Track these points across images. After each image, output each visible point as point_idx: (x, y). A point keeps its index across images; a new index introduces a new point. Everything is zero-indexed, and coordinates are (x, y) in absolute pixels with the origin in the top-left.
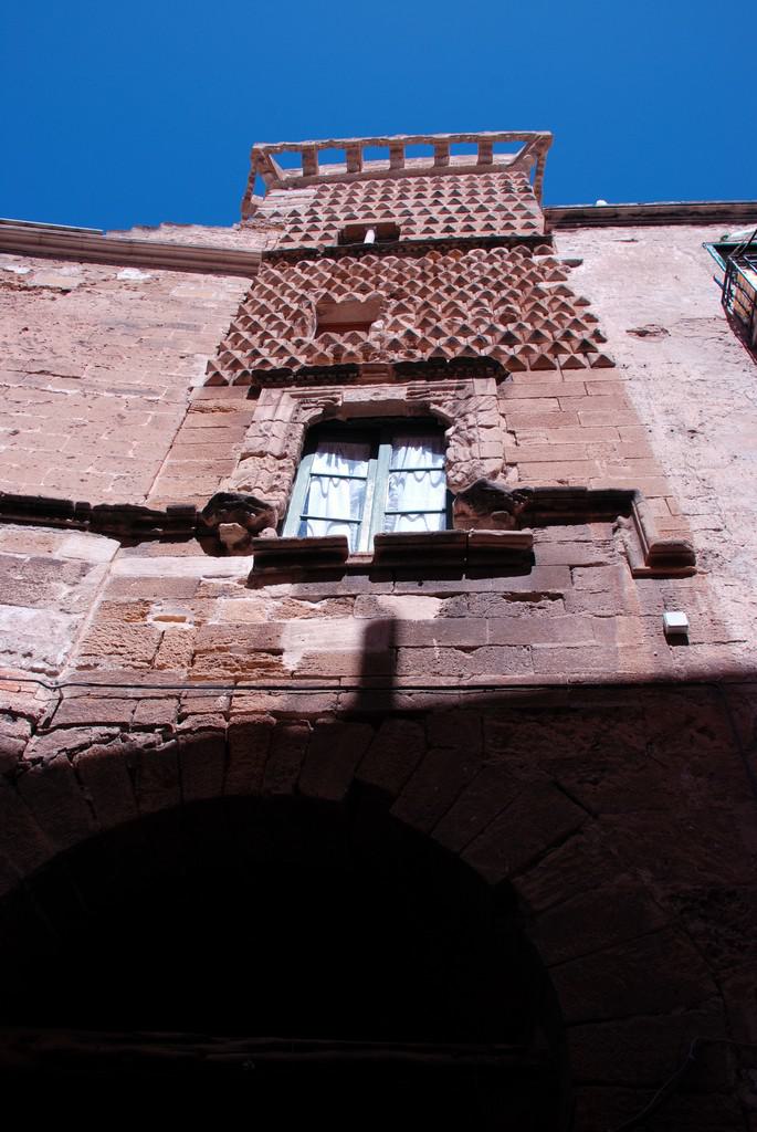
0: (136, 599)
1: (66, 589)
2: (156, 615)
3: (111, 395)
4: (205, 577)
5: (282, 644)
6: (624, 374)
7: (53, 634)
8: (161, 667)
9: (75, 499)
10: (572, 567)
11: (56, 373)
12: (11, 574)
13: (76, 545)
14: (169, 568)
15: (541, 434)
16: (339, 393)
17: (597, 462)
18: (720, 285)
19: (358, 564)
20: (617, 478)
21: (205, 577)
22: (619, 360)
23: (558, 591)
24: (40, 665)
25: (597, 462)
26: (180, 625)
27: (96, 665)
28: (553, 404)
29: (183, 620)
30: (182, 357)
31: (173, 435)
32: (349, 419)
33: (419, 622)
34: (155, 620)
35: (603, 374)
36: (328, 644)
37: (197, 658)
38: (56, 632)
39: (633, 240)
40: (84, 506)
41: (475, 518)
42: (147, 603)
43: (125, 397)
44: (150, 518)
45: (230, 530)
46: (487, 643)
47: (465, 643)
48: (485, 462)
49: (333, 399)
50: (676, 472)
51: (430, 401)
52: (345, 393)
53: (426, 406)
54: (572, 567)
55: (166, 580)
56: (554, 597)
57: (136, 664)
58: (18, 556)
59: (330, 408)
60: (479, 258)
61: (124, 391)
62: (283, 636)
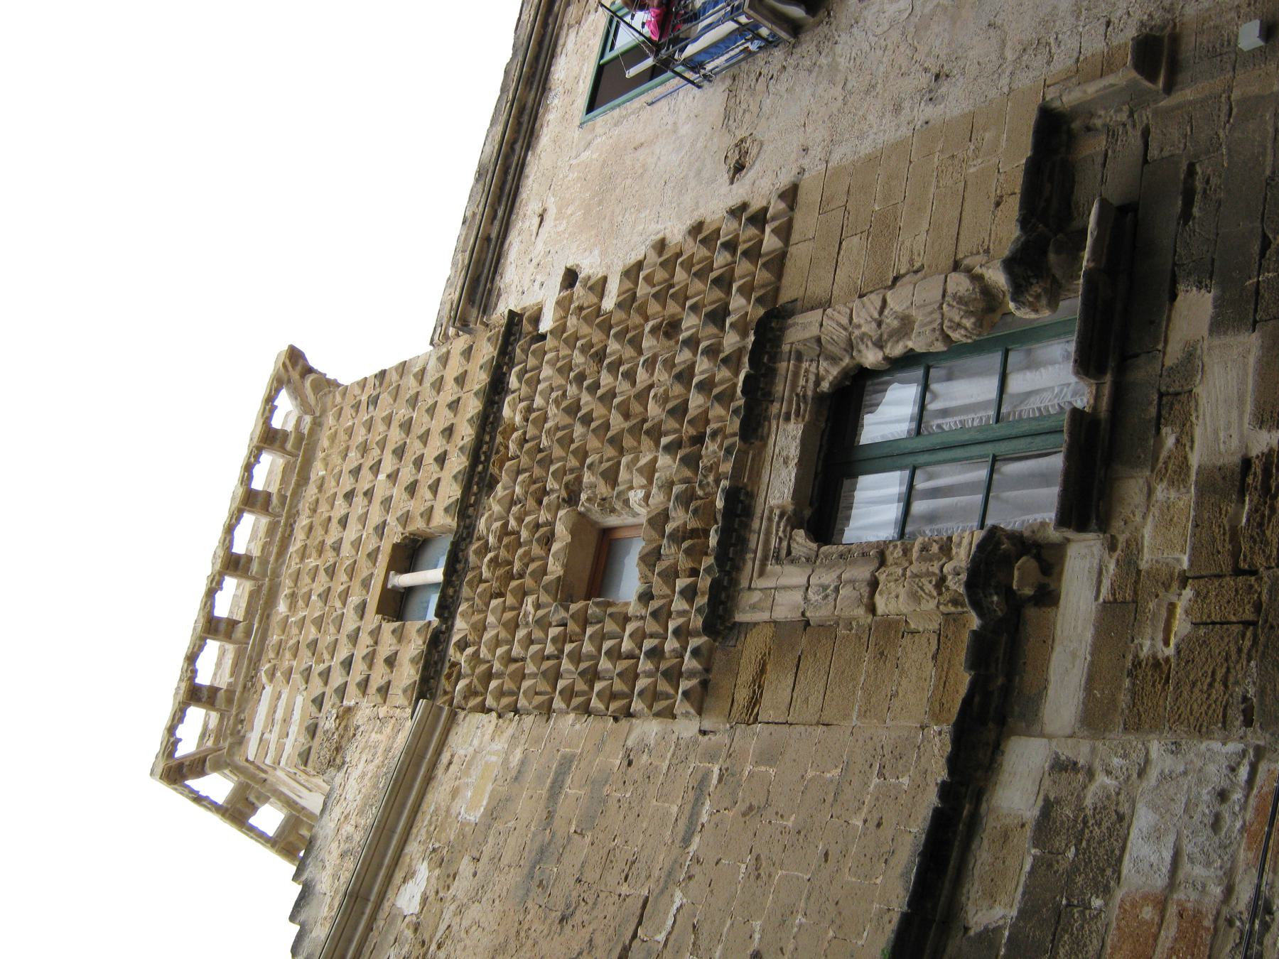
1: (1102, 779)
2: (1160, 644)
3: (696, 839)
4: (1097, 598)
5: (1237, 459)
6: (814, 167)
8: (1258, 607)
9: (931, 798)
11: (629, 934)
12: (1063, 866)
13: (1018, 788)
14: (1074, 655)
15: (907, 244)
16: (771, 511)
17: (972, 170)
20: (1004, 144)
21: (1097, 598)
23: (1185, 168)
24: (1244, 772)
25: (972, 170)
29: (1172, 607)
30: (630, 764)
32: (811, 504)
33: (1215, 307)
35: (809, 196)
36: (1241, 401)
37: (1244, 566)
39: (542, 217)
40: (946, 791)
42: (1137, 664)
44: (977, 699)
45: (1022, 576)
46: (1258, 224)
47: (1256, 248)
49: (781, 516)
50: (1005, 81)
52: (773, 502)
53: (820, 398)
54: (1145, 161)
56: (1191, 172)
57: (1248, 643)
58: (1027, 867)
61: (694, 815)
62: (1219, 464)
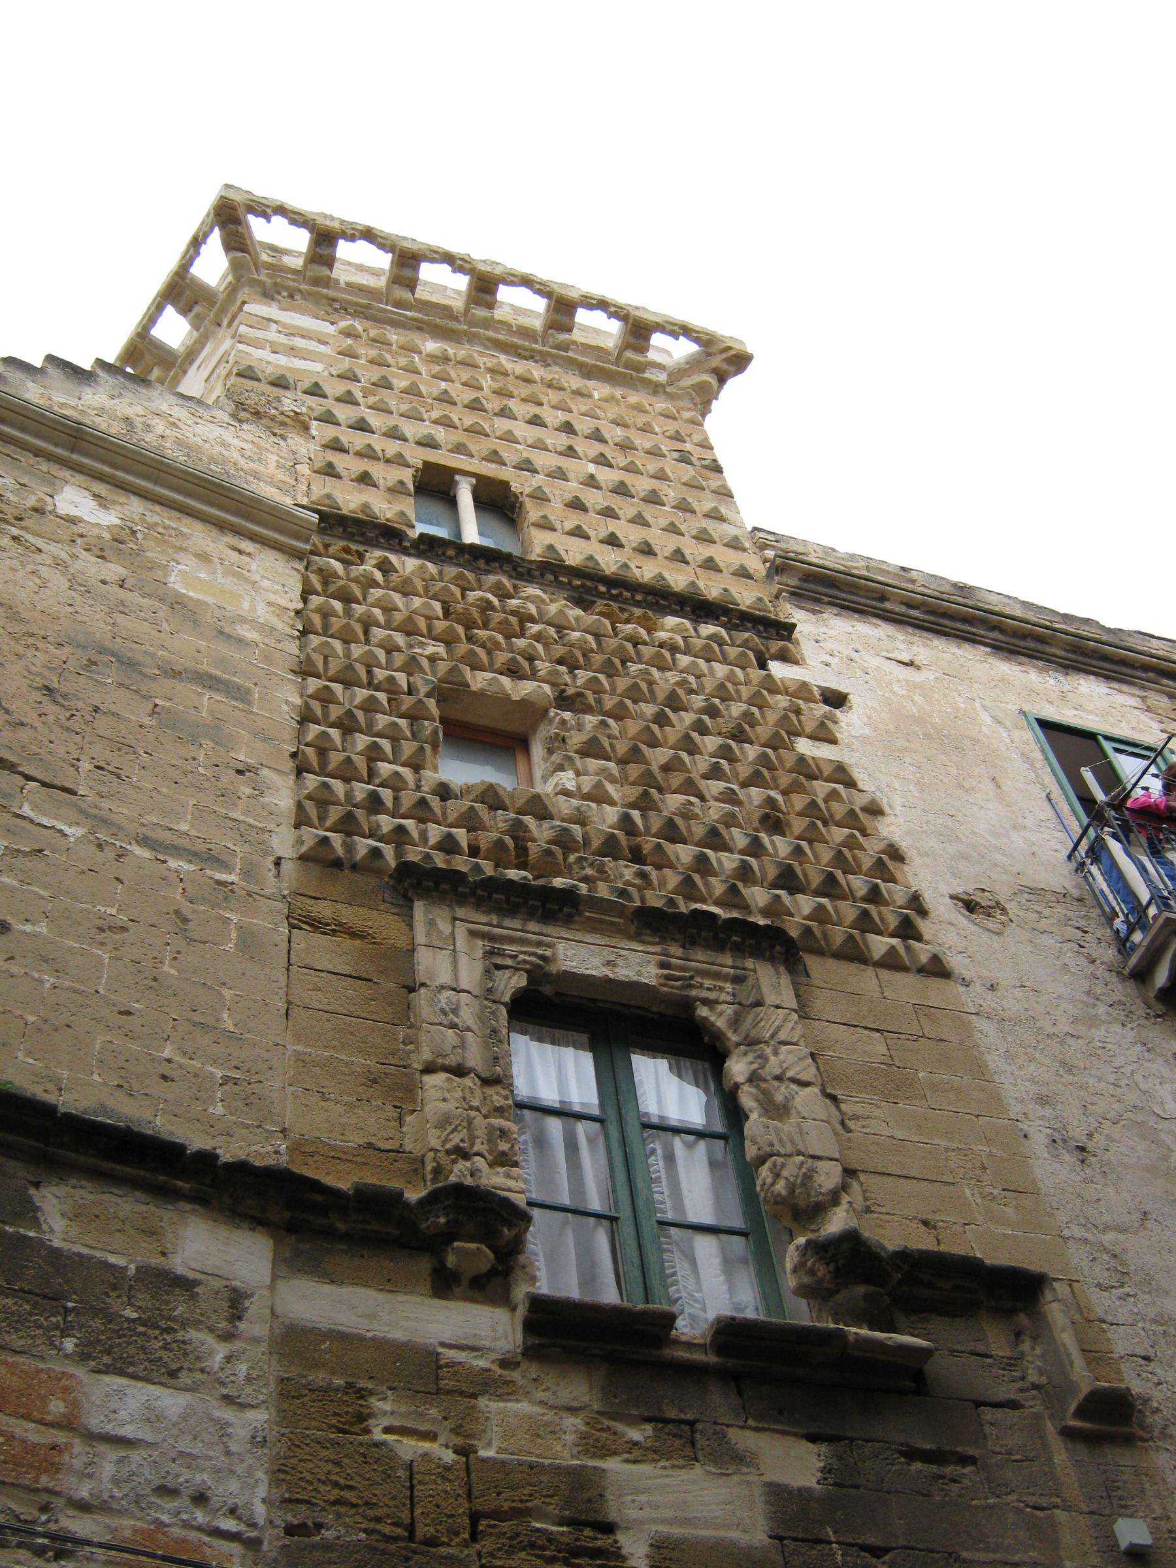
0: (339, 1382)
1: (221, 1351)
3: (146, 854)
5: (613, 1516)
6: (970, 998)
7: (228, 1453)
8: (431, 1542)
10: (978, 1404)
13: (205, 1246)
16: (550, 945)
18: (1081, 826)
19: (1105, 1389)
22: (955, 962)
24: (230, 1525)
25: (967, 1192)
26: (427, 1445)
27: (319, 1526)
28: (878, 1046)
29: (431, 1436)
30: (240, 772)
31: (283, 982)
33: (799, 1490)
34: (388, 1430)
35: (936, 991)
38: (234, 1448)
40: (206, 1159)
41: (831, 1286)
42: (362, 1394)
43: (173, 863)
44: (319, 1198)
47: (872, 1540)
48: (820, 1164)
50: (1078, 1232)
51: (697, 999)
52: (561, 947)
53: (688, 1005)
54: (978, 1404)
55: (380, 1344)
59: (537, 975)
60: (325, 583)
61: (176, 850)
